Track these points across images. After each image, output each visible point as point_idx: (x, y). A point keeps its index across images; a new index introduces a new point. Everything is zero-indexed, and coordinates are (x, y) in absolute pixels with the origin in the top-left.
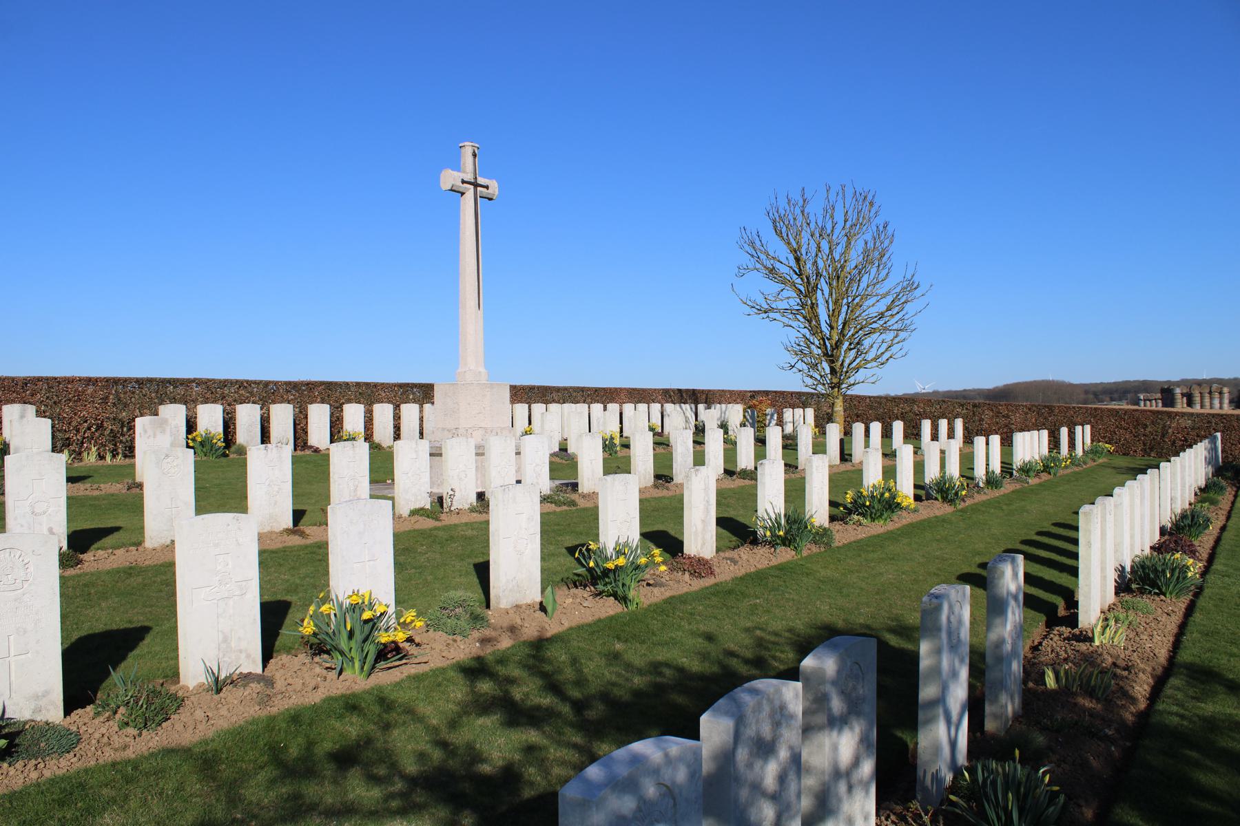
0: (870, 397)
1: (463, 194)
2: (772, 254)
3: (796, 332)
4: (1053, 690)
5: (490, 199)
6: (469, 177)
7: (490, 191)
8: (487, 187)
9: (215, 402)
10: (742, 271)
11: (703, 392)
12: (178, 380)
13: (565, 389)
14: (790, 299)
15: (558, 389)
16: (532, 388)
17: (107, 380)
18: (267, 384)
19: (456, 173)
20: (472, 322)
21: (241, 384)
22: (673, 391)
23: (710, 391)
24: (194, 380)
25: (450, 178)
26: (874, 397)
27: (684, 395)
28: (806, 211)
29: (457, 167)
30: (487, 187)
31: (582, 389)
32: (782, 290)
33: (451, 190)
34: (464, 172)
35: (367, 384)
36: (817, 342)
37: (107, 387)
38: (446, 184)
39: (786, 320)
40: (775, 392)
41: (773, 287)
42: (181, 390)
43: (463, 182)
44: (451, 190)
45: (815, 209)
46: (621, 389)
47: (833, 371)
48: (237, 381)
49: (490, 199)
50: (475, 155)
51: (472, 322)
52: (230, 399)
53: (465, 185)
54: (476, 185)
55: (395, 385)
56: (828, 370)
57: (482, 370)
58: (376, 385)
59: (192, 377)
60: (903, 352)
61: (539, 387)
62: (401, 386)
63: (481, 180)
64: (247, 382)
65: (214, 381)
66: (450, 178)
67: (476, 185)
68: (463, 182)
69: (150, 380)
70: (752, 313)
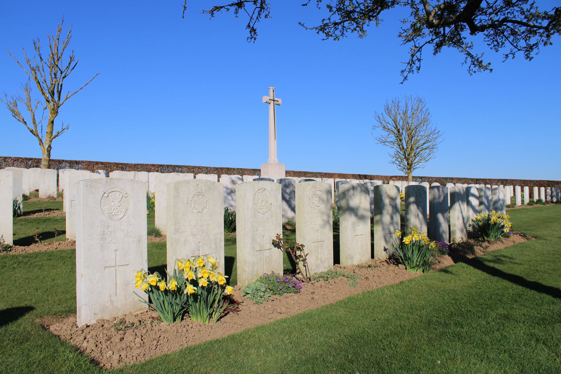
0: (436, 178)
1: (270, 104)
2: (386, 121)
3: (393, 150)
4: (452, 248)
5: (279, 105)
6: (272, 98)
7: (279, 102)
8: (278, 101)
9: (191, 172)
10: (374, 128)
11: (369, 176)
12: (179, 166)
13: (313, 173)
14: (392, 138)
15: (311, 173)
16: (300, 172)
17: (158, 165)
18: (207, 168)
19: (267, 97)
20: (273, 145)
21: (199, 168)
22: (357, 175)
23: (372, 175)
24: (184, 166)
25: (265, 99)
26: (437, 178)
27: (361, 176)
28: (399, 105)
29: (268, 95)
30: (278, 101)
31: (320, 173)
32: (389, 134)
33: (266, 102)
34: (270, 97)
35: (241, 169)
36: (402, 153)
37: (157, 167)
38: (264, 101)
39: (391, 146)
40: (399, 176)
41: (385, 133)
42: (180, 169)
43: (270, 100)
44: (266, 102)
45: (402, 105)
46: (335, 174)
47: (408, 164)
48: (198, 167)
49: (279, 105)
50: (273, 91)
51: (273, 145)
52: (196, 172)
53: (271, 101)
54: (274, 101)
55: (251, 169)
56: (406, 164)
57: (276, 160)
58: (244, 169)
59: (184, 165)
60: (434, 157)
61: (303, 172)
62: (253, 170)
63: (276, 99)
64: (201, 167)
65: (191, 166)
66: (265, 99)
67: (274, 101)
68: (270, 100)
69: (171, 166)
70: (379, 143)
